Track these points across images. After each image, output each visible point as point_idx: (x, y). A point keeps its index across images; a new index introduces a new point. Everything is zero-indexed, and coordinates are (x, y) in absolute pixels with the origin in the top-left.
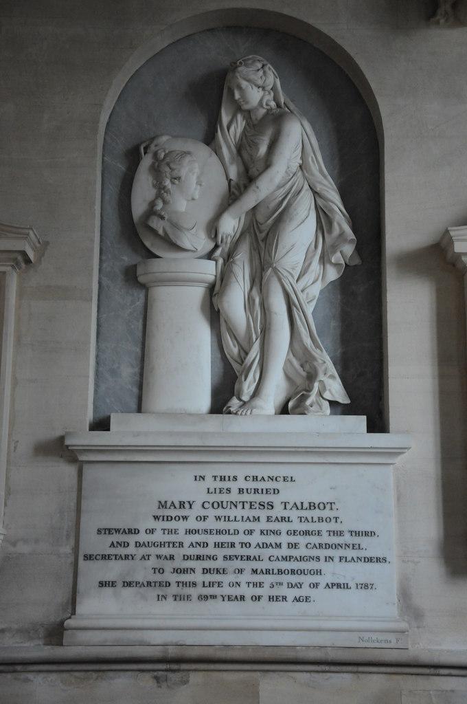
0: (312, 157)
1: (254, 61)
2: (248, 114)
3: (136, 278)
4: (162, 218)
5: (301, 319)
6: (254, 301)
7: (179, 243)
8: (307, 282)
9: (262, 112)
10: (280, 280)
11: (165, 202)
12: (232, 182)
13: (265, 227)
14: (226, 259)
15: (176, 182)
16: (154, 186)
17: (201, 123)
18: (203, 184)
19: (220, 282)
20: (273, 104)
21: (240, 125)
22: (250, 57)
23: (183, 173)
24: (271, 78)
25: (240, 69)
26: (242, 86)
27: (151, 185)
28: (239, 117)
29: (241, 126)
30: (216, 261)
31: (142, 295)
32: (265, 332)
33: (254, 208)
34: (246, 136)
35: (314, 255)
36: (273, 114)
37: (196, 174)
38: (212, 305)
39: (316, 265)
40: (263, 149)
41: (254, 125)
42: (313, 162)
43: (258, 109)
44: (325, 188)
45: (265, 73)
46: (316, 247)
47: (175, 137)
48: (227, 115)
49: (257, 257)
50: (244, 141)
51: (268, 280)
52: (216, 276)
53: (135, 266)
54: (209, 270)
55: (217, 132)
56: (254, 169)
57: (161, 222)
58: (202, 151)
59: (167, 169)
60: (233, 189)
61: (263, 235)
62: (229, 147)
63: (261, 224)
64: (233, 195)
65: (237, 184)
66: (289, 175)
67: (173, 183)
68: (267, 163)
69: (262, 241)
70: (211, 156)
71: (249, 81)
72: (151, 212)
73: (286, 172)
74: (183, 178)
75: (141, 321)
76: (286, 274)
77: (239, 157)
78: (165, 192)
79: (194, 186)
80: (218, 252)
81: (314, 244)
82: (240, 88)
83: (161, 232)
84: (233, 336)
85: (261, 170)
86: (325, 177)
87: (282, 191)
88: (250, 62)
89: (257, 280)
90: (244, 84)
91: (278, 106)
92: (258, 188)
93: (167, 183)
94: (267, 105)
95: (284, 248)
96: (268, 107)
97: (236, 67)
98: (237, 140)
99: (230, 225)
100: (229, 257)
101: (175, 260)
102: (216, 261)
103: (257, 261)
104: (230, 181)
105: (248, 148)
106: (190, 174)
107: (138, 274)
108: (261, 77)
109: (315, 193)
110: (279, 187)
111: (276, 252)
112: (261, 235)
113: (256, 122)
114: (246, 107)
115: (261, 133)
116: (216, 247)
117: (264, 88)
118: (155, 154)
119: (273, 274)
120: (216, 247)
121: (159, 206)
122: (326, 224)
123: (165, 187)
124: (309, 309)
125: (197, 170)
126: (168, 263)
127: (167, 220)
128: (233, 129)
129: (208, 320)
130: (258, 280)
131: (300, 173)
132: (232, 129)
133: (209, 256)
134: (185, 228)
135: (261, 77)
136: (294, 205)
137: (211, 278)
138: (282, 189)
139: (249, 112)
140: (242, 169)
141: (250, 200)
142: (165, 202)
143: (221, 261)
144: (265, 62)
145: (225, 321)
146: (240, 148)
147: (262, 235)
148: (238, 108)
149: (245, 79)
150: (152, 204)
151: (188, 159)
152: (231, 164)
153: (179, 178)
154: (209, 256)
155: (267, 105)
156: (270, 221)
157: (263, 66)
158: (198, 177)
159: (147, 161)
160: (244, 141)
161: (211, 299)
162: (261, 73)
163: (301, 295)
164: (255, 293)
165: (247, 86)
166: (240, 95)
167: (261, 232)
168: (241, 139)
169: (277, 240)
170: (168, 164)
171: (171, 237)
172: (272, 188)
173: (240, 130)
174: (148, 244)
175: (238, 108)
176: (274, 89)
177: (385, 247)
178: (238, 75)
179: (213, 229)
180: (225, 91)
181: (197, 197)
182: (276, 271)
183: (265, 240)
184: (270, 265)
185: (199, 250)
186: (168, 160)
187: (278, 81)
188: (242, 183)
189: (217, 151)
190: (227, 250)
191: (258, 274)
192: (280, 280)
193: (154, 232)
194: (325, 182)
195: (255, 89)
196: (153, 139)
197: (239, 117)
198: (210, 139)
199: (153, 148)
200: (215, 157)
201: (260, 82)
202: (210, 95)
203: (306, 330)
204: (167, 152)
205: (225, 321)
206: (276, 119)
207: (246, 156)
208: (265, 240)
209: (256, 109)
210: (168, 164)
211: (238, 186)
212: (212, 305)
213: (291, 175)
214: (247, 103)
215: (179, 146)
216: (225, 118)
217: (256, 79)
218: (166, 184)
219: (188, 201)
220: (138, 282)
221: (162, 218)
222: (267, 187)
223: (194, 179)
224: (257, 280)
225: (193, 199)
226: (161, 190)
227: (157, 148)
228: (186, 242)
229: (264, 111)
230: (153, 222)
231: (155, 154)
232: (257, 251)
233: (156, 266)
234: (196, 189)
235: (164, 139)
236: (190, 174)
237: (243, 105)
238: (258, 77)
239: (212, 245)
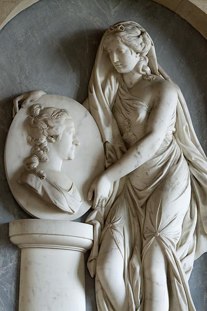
0: (186, 126)
1: (133, 28)
2: (121, 77)
3: (8, 238)
4: (41, 176)
5: (181, 291)
6: (134, 270)
7: (59, 204)
8: (183, 254)
9: (138, 76)
10: (163, 250)
11: (41, 160)
12: (107, 144)
13: (144, 194)
14: (103, 222)
15: (53, 140)
16: (29, 142)
17: (71, 81)
18: (79, 144)
19: (97, 247)
20: (148, 70)
21: (113, 87)
22: (129, 22)
23: (61, 131)
24: (150, 45)
25: (122, 34)
26: (123, 50)
27: (25, 140)
28: (113, 79)
29: (115, 88)
30: (94, 225)
31: (14, 256)
32: (144, 301)
33: (132, 173)
34: (120, 98)
35: (191, 226)
36: (150, 80)
37: (72, 133)
38: (87, 271)
39: (191, 239)
40: (143, 115)
41: (129, 89)
42: (187, 131)
43: (134, 74)
44: (198, 158)
45: (144, 40)
46: (192, 217)
47: (48, 93)
48: (100, 76)
49: (136, 224)
50: (118, 101)
51: (151, 250)
52: (93, 241)
53: (8, 223)
54: (86, 234)
55: (92, 92)
56: (130, 134)
57: (40, 180)
58: (76, 112)
59: (45, 126)
60: (108, 152)
61: (143, 201)
62: (104, 108)
63: (140, 190)
64: (109, 159)
65: (113, 147)
66: (167, 143)
67: (49, 141)
68: (147, 131)
69: (142, 207)
70: (86, 116)
71: (129, 46)
72: (27, 169)
73: (164, 140)
74: (60, 137)
75: (14, 284)
76: (169, 244)
77: (114, 120)
78: (41, 149)
79: (71, 145)
80: (93, 216)
81: (189, 213)
82: (119, 52)
83: (40, 192)
84: (109, 304)
85: (139, 137)
86: (197, 147)
87: (162, 159)
88: (130, 28)
89: (137, 248)
90: (125, 48)
91: (153, 72)
92: (139, 153)
93: (44, 140)
94: (143, 70)
95: (167, 217)
96: (144, 73)
97: (119, 32)
98: (111, 102)
99: (106, 188)
100: (107, 221)
101: (55, 221)
102: (94, 225)
103: (136, 227)
104: (105, 143)
105: (124, 111)
106: (67, 134)
107: (10, 235)
108: (141, 44)
109: (189, 163)
110: (158, 155)
111: (159, 221)
112: (140, 201)
113: (130, 86)
114: (123, 71)
115: (140, 98)
116: (91, 210)
117: (141, 54)
118: (31, 110)
119: (156, 243)
120: (91, 210)
121: (36, 164)
122: (201, 196)
123: (41, 145)
124: (187, 278)
125: (73, 130)
126: (46, 222)
127: (46, 179)
128: (107, 91)
129: (83, 286)
130: (139, 247)
131: (175, 142)
132: (107, 91)
133: (84, 219)
134: (64, 189)
135: (141, 44)
136: (174, 174)
137: (88, 242)
138: (161, 157)
139: (122, 75)
140: (117, 131)
141: (129, 165)
142: (41, 160)
143: (98, 225)
144: (144, 30)
145: (102, 289)
146: (114, 109)
147: (142, 203)
148: (112, 70)
149: (126, 45)
150: (28, 162)
151: (64, 118)
152: (107, 125)
153: (56, 137)
154: (84, 219)
155: (143, 70)
156: (150, 189)
157: (142, 33)
158: (74, 137)
159: (21, 116)
160: (118, 101)
161: (86, 265)
162: (141, 40)
163: (181, 265)
164: (135, 261)
165: (126, 51)
166: (119, 58)
167: (139, 199)
168: (115, 101)
169: (161, 209)
170: (46, 121)
171: (51, 197)
172: (152, 155)
173: (113, 93)
174: (22, 202)
175: (112, 70)
176: (149, 55)
177: (81, 195)
178: (119, 39)
179: (89, 191)
180: (100, 53)
181: (73, 157)
182: (159, 240)
183: (144, 206)
184: (153, 233)
185: (76, 212)
186: (45, 116)
187: (153, 48)
188: (117, 147)
189: (92, 111)
190: (102, 214)
191: (138, 242)
192: (163, 250)
193: (32, 191)
194: (198, 152)
195: (134, 54)
196: (29, 93)
197: (113, 79)
198: (83, 96)
199: (28, 103)
200: (90, 117)
201: (140, 49)
202: (83, 54)
203: (186, 304)
204: (43, 108)
205: (102, 289)
206: (154, 88)
207: (121, 118)
208: (144, 206)
209: (131, 73)
210: (46, 121)
211: (113, 150)
212: (87, 271)
213: (169, 143)
214: (125, 67)
215: (54, 103)
216: (100, 79)
217: (137, 45)
218: (43, 141)
219: (64, 160)
220: (11, 242)
221: (41, 176)
222: (148, 153)
223: (70, 139)
224: (137, 248)
225: (69, 159)
226: (36, 148)
227: (32, 104)
228: (64, 205)
229: (141, 75)
230: (32, 180)
231: (31, 110)
232: (136, 217)
233: (34, 227)
234: (72, 148)
235: (40, 94)
236: (67, 134)
237: (120, 68)
238: (137, 43)
239: (89, 207)
